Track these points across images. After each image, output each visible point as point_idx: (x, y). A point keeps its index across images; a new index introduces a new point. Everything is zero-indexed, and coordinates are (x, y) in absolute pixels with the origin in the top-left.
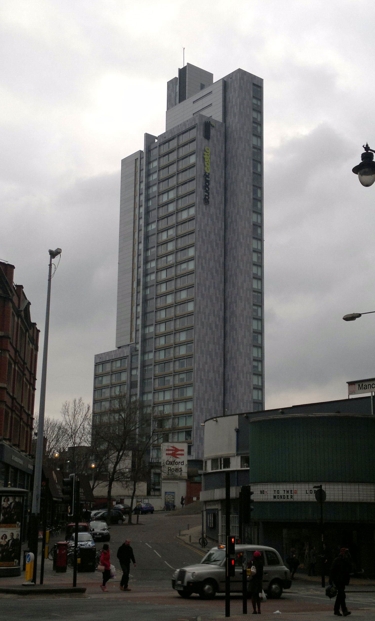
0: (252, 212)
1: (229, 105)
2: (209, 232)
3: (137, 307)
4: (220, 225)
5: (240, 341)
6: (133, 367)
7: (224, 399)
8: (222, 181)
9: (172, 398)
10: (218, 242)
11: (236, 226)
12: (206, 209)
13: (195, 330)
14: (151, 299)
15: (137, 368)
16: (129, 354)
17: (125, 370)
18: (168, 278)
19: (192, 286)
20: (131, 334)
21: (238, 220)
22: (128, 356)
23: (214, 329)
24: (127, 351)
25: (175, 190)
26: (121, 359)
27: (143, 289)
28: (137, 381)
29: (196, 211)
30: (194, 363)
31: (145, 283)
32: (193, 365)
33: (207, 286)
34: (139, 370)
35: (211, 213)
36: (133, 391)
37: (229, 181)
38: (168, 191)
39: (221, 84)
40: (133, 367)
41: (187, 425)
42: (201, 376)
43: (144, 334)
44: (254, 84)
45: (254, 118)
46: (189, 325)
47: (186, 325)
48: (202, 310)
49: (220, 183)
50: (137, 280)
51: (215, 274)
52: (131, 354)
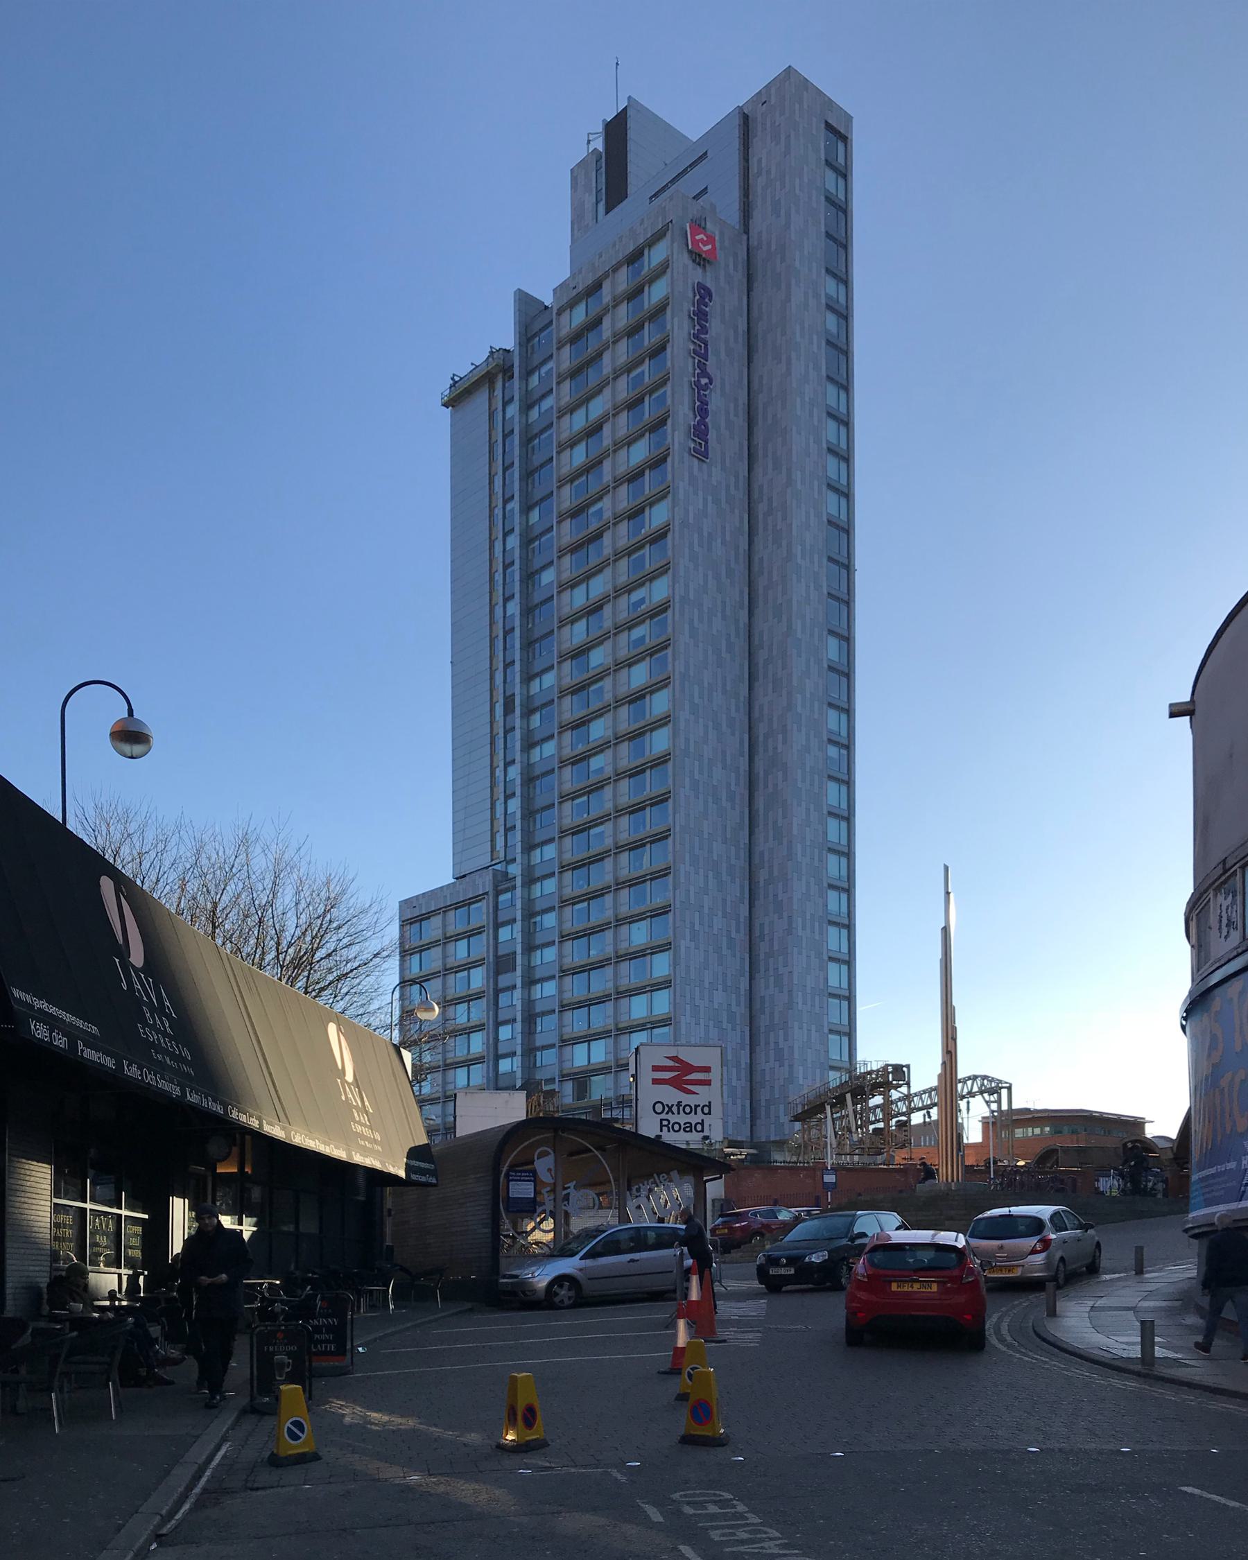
0: (825, 706)
1: (758, 184)
2: (710, 534)
3: (506, 802)
4: (736, 889)
5: (795, 832)
6: (501, 1018)
7: (749, 400)
8: (742, 325)
9: (611, 1057)
10: (734, 1008)
11: (785, 817)
12: (700, 469)
13: (674, 877)
14: (544, 1014)
15: (514, 1020)
16: (489, 888)
17: (479, 1028)
18: (591, 457)
19: (663, 911)
20: (493, 840)
21: (789, 727)
22: (487, 893)
23: (724, 803)
24: (485, 883)
25: (609, 716)
26: (468, 903)
27: (522, 717)
28: (515, 953)
29: (675, 1004)
30: (673, 431)
31: (529, 969)
32: (670, 668)
33: (706, 910)
34: (518, 926)
35: (715, 632)
36: (504, 980)
37: (761, 399)
38: (588, 578)
39: (737, 121)
40: (500, 920)
41: (655, 976)
42: (693, 924)
43: (529, 731)
44: (829, 126)
45: (828, 296)
46: (657, 866)
47: (647, 492)
48: (692, 750)
49: (736, 400)
50: (505, 698)
51: (725, 951)
52: (496, 887)
